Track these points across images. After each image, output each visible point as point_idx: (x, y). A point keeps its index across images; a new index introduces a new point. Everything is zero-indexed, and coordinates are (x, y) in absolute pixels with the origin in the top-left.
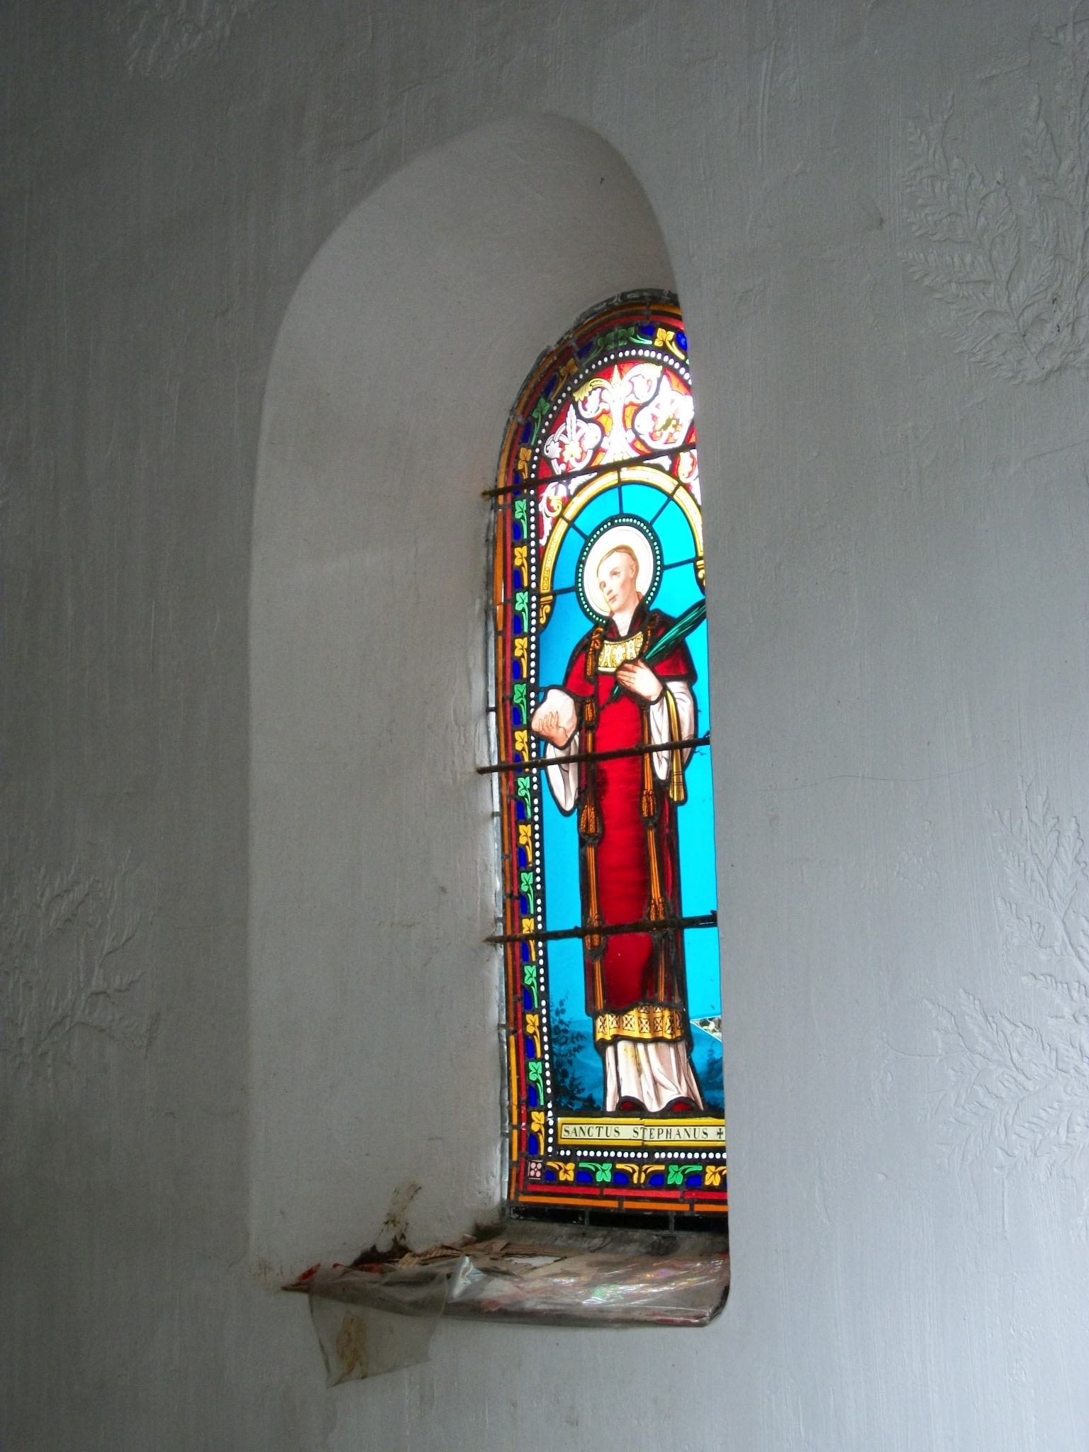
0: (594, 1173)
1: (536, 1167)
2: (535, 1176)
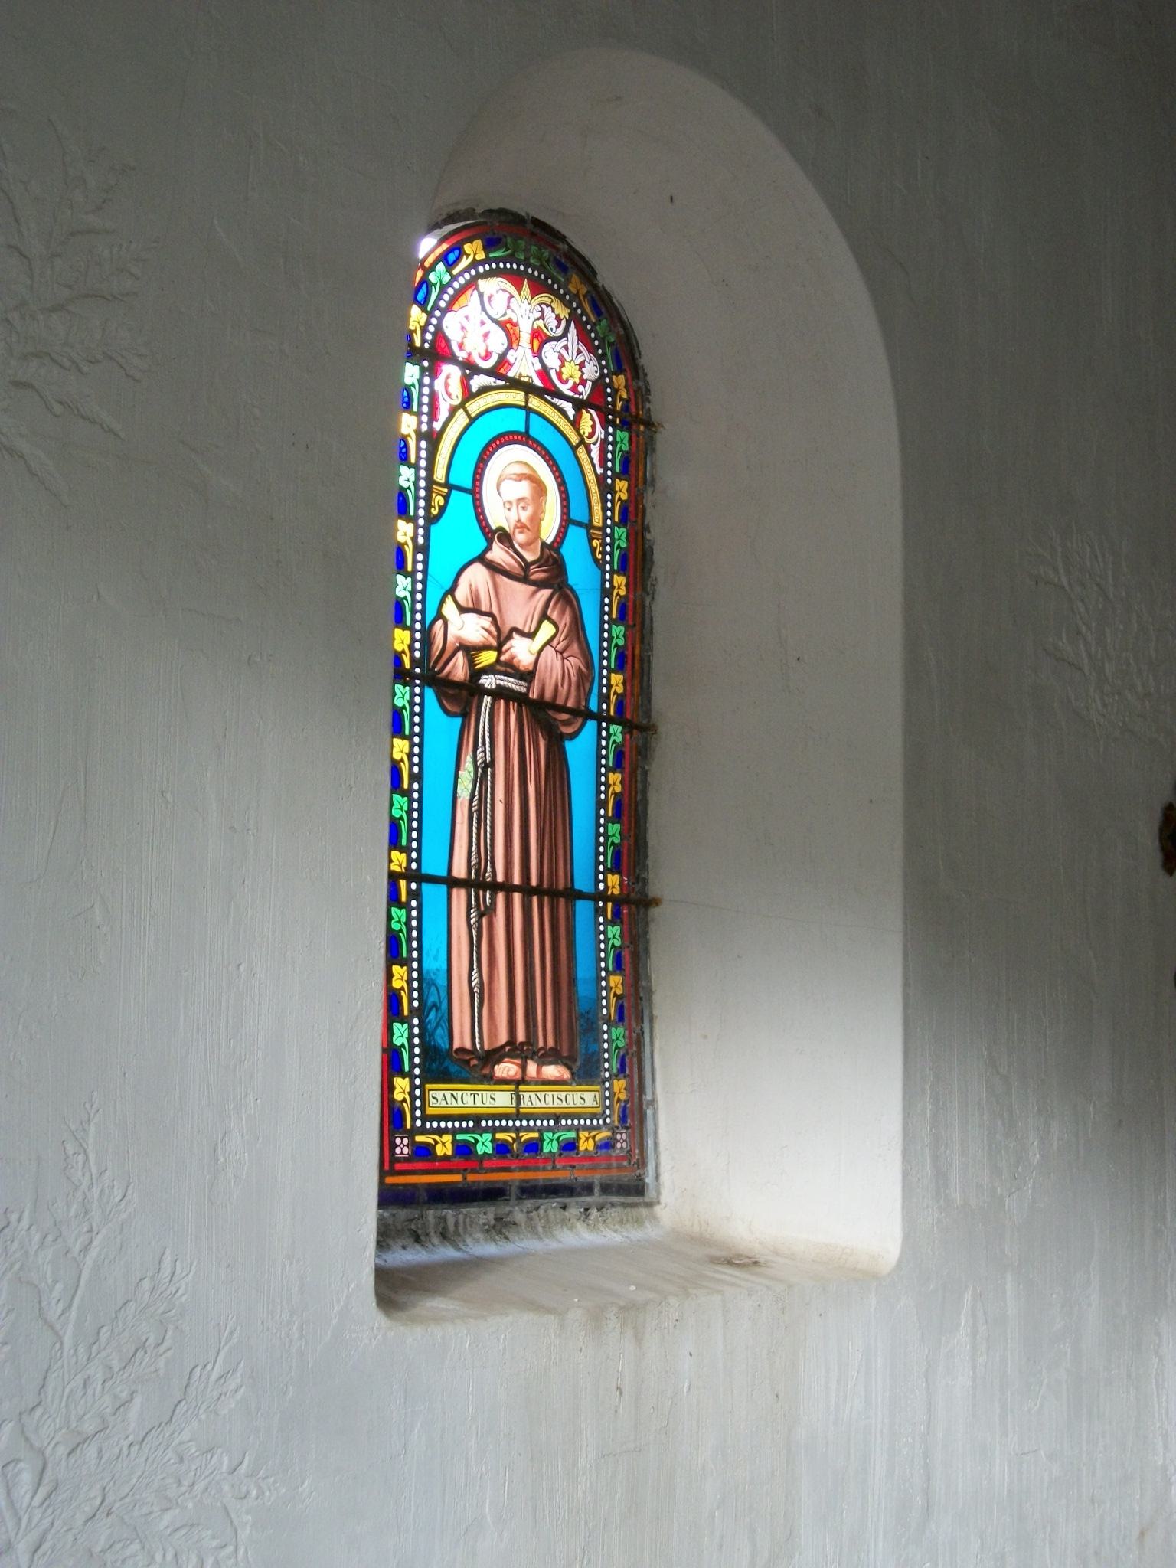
0: (434, 1147)
1: (402, 1149)
2: (402, 1138)
